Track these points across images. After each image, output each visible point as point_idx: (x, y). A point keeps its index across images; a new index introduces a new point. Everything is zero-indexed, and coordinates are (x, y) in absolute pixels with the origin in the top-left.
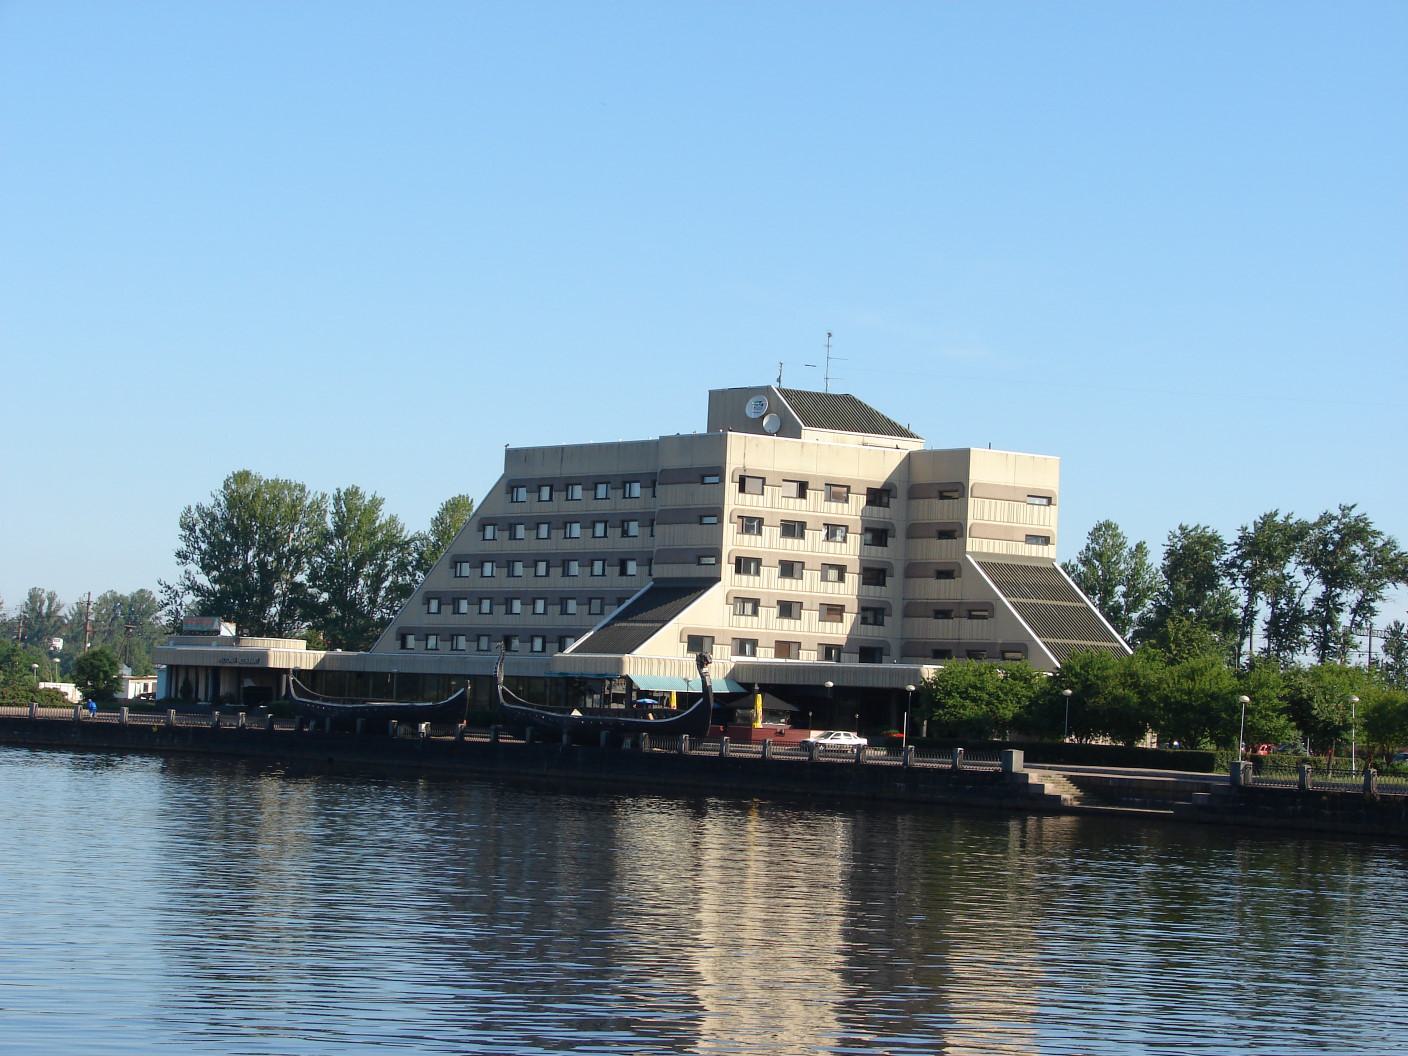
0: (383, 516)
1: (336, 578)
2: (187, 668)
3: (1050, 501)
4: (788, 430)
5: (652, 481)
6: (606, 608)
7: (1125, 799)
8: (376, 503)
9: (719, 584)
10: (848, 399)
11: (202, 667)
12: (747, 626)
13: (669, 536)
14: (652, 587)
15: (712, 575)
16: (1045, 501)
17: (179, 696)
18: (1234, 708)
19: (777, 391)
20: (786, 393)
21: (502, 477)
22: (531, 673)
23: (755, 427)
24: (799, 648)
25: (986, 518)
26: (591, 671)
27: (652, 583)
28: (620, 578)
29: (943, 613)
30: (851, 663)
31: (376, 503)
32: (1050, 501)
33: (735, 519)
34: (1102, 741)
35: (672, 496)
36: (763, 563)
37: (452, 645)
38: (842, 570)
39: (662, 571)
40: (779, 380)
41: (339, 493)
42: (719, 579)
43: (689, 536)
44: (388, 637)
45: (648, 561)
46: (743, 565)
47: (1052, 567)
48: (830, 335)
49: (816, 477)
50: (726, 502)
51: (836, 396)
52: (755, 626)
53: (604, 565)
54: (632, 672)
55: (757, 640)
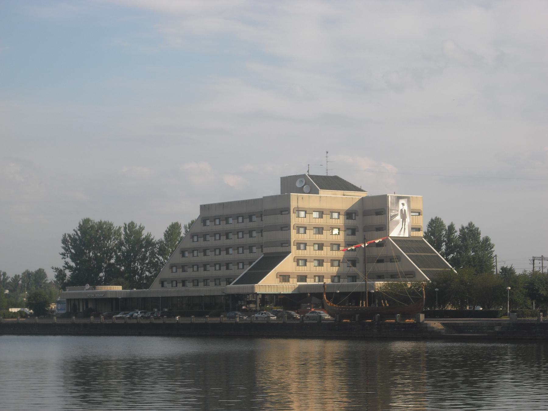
0: (144, 233)
1: (127, 259)
2: (75, 299)
3: (420, 214)
4: (313, 191)
5: (261, 215)
6: (245, 266)
7: (466, 331)
8: (142, 229)
9: (291, 254)
10: (336, 178)
11: (77, 299)
12: (302, 270)
13: (268, 236)
14: (263, 257)
15: (288, 251)
16: (417, 214)
17: (72, 311)
18: (506, 292)
19: (308, 176)
20: (310, 176)
21: (199, 217)
22: (216, 294)
23: (300, 190)
24: (289, 278)
25: (414, 223)
26: (241, 292)
27: (263, 255)
28: (204, 257)
29: (380, 261)
30: (345, 282)
31: (142, 229)
32: (420, 214)
33: (295, 228)
34: (449, 308)
35: (269, 220)
36: (307, 244)
37: (204, 283)
38: (339, 245)
39: (266, 250)
40: (308, 171)
41: (126, 225)
42: (290, 252)
43: (279, 235)
44: (156, 282)
45: (261, 247)
46: (298, 245)
47: (422, 240)
48: (327, 152)
49: (326, 209)
50: (291, 221)
51: (331, 177)
52: (306, 270)
53: (197, 252)
54: (258, 291)
55: (307, 276)
